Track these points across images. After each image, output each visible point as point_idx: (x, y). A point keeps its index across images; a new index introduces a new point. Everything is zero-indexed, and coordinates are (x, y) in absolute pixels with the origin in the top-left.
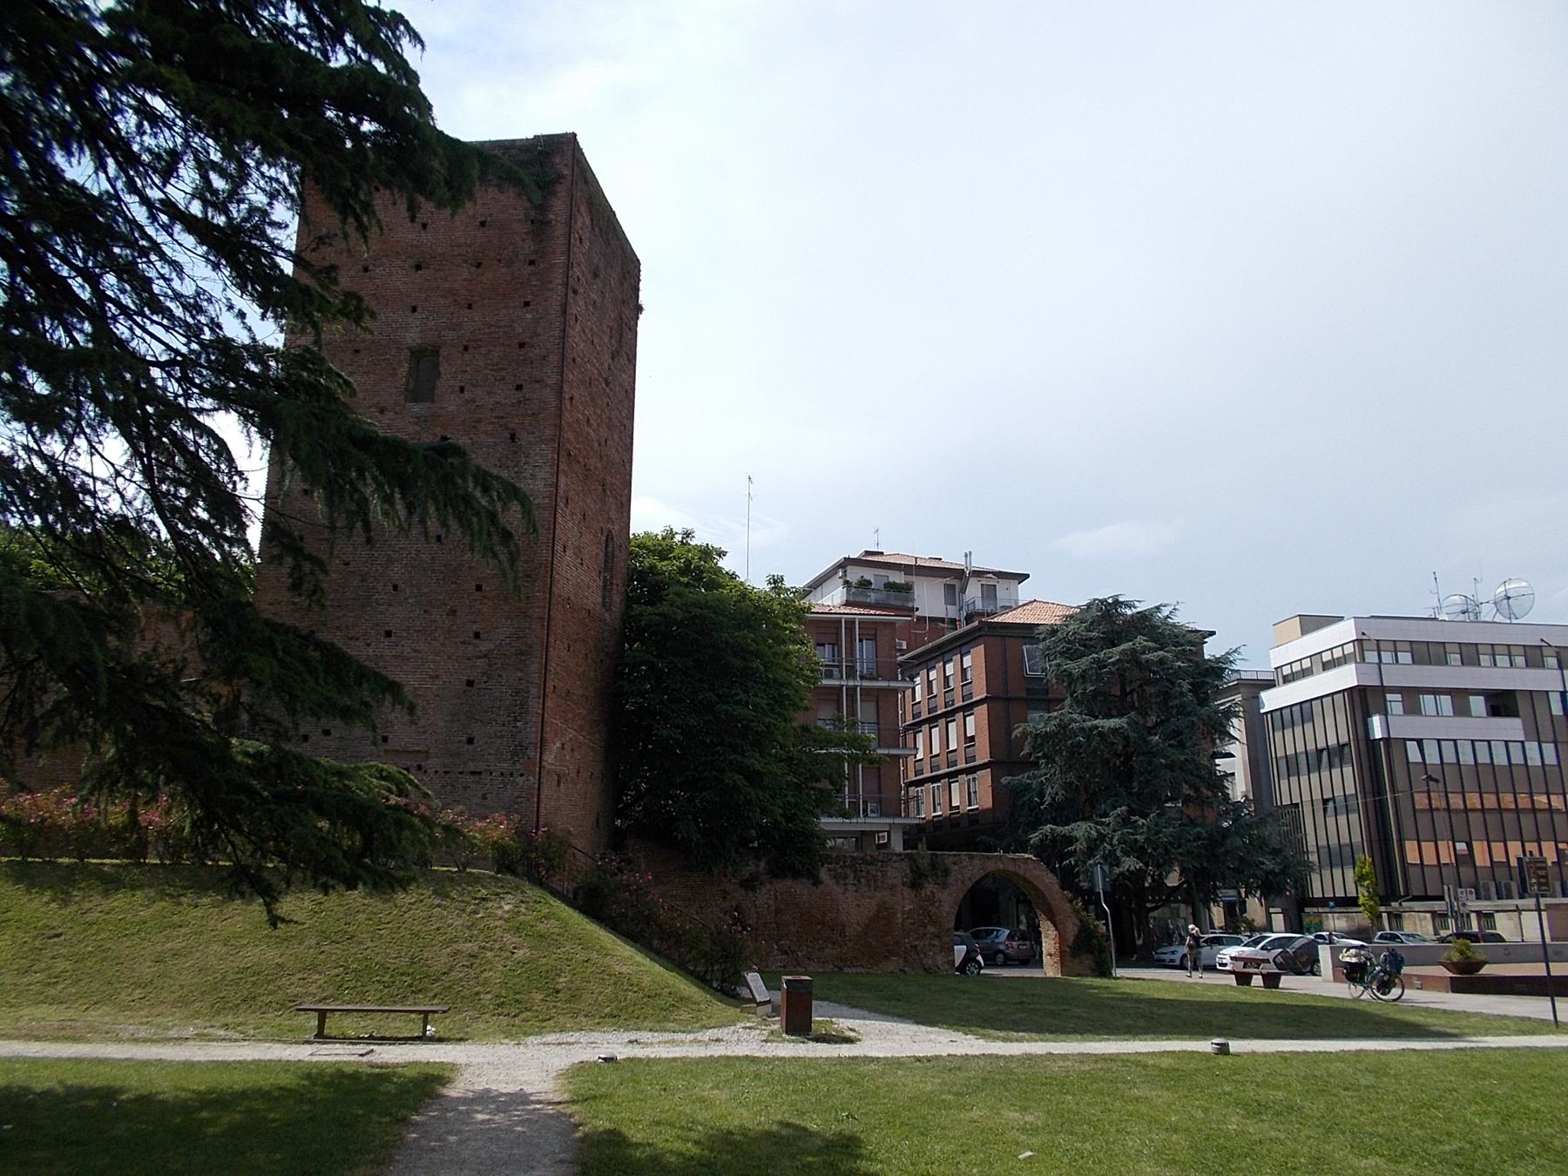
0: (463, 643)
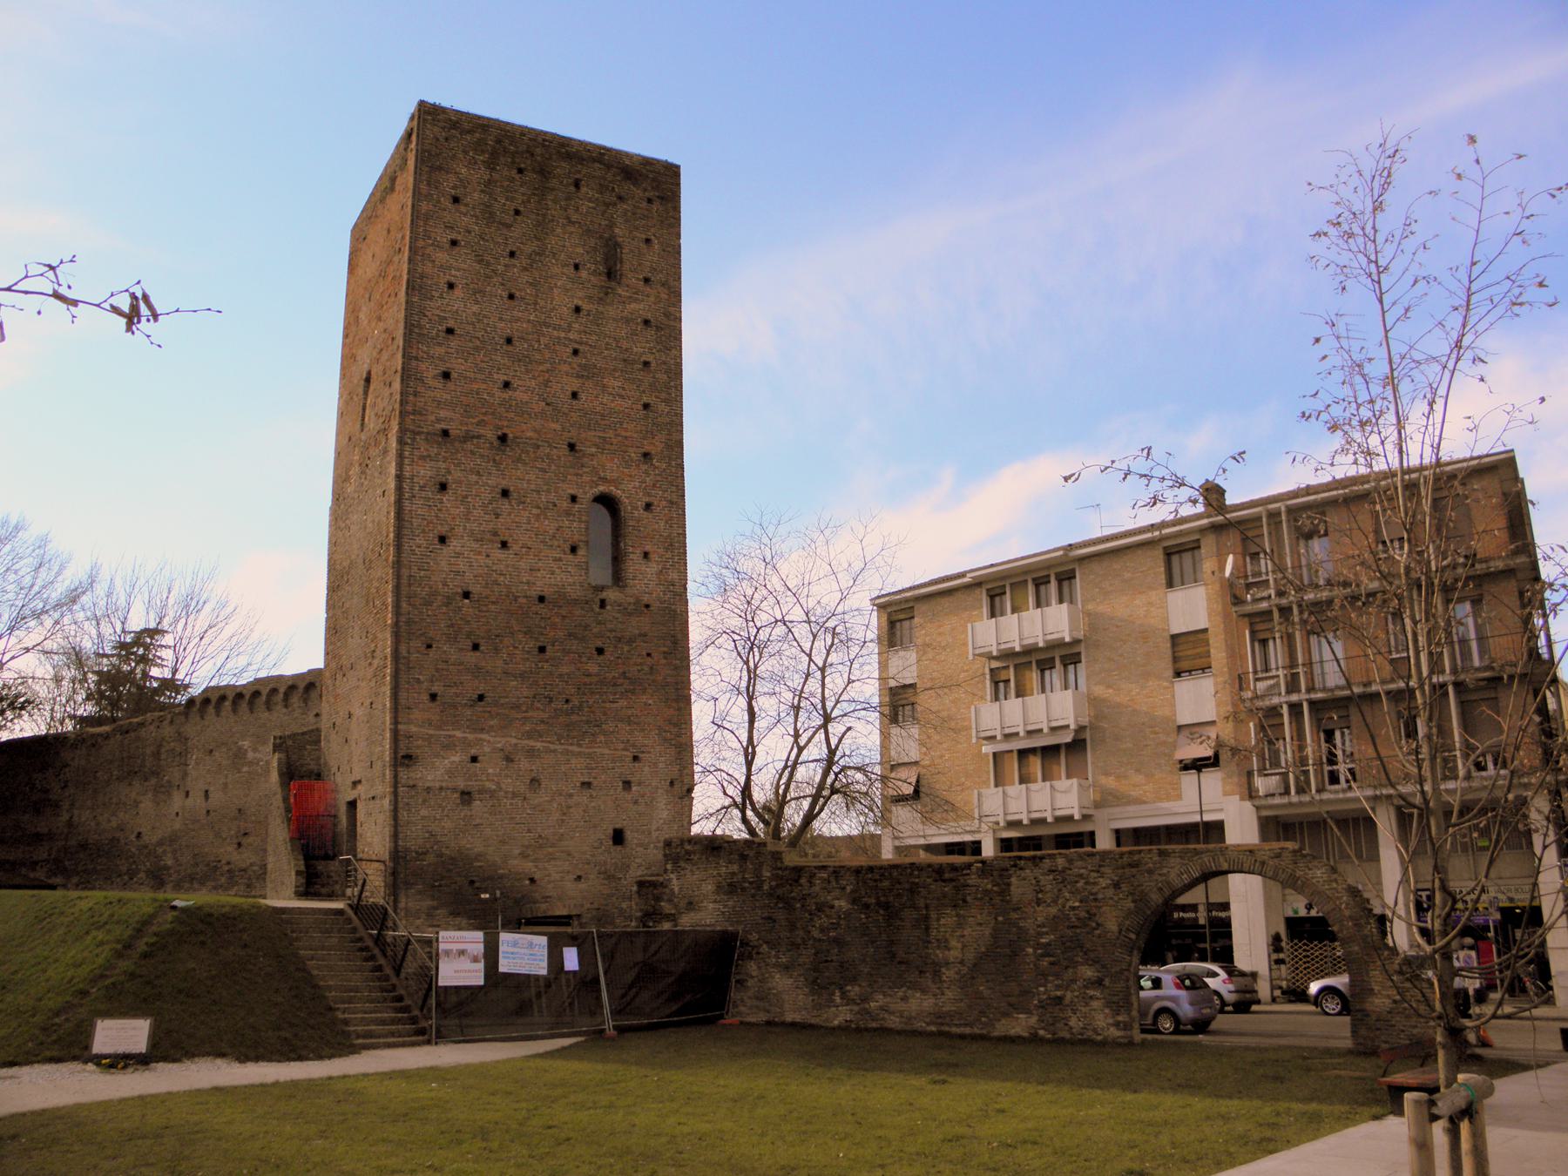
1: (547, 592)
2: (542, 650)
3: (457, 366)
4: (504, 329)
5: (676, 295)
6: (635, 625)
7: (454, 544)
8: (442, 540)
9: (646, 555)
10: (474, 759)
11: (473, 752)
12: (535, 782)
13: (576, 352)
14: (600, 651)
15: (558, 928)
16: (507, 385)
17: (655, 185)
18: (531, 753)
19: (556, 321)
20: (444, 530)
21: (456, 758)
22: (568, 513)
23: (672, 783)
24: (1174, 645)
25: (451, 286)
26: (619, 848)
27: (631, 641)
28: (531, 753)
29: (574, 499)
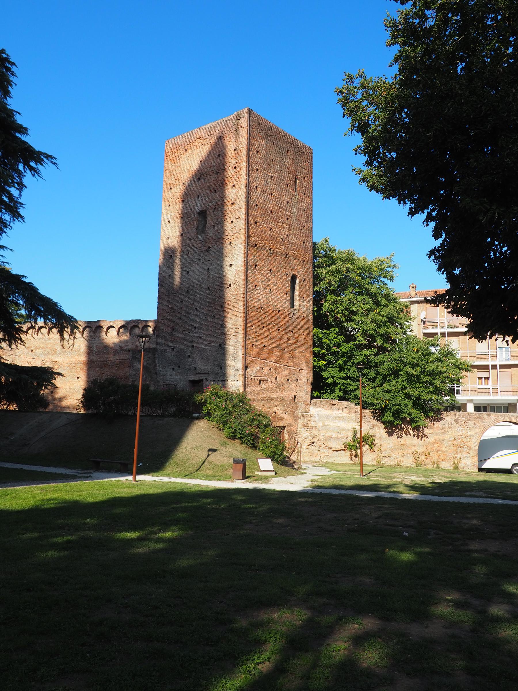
0: (218, 329)
11: (262, 366)
28: (276, 369)
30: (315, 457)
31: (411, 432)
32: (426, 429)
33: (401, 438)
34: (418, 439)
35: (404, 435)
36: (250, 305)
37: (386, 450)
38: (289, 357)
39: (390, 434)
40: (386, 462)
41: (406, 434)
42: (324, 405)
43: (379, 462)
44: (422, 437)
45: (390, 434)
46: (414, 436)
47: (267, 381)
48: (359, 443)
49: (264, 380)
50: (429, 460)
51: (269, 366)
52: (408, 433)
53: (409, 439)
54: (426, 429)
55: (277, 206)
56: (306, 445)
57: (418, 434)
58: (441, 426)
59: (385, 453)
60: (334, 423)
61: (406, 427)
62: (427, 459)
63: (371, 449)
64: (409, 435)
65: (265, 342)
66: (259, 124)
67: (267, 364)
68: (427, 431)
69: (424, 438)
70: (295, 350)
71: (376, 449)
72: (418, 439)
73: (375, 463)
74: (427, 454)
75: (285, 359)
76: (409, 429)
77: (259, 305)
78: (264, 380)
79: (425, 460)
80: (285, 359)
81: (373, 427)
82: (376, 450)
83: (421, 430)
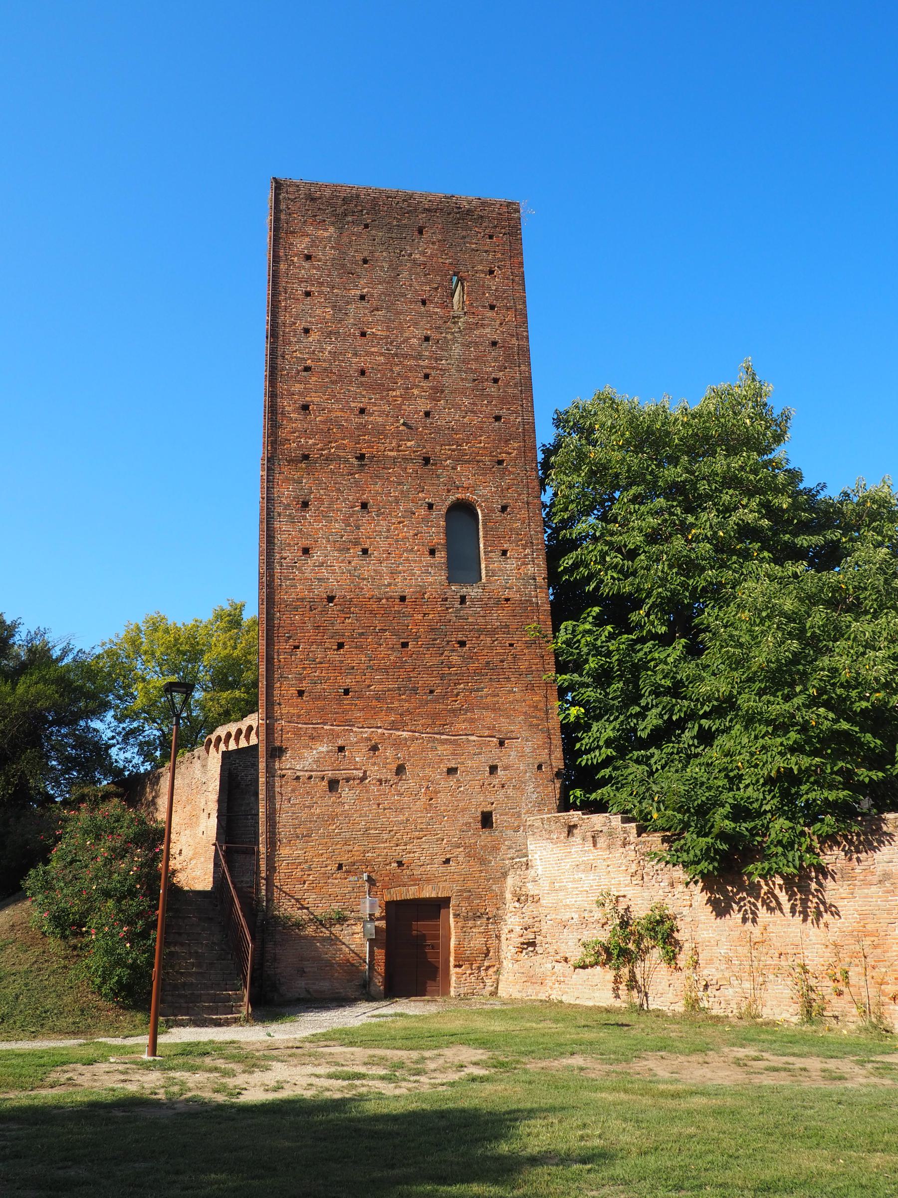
1: (407, 592)
2: (405, 645)
3: (314, 398)
4: (358, 362)
5: (523, 316)
6: (498, 617)
7: (317, 556)
8: (306, 551)
9: (504, 553)
10: (341, 749)
11: (340, 742)
12: (400, 770)
13: (427, 376)
14: (462, 644)
15: (267, 906)
16: (362, 411)
17: (501, 225)
18: (398, 744)
19: (405, 349)
20: (305, 543)
21: (324, 749)
22: (425, 520)
23: (540, 767)
24: (457, 216)
25: (307, 331)
26: (487, 831)
27: (494, 631)
28: (398, 744)
29: (430, 506)
30: (537, 987)
31: (783, 897)
32: (829, 883)
33: (754, 921)
34: (805, 920)
35: (762, 912)
36: (284, 595)
37: (710, 961)
38: (453, 711)
39: (721, 909)
40: (713, 1004)
41: (771, 909)
42: (550, 832)
43: (693, 1004)
44: (819, 915)
45: (721, 909)
46: (793, 911)
47: (363, 779)
48: (631, 943)
49: (348, 780)
50: (847, 997)
51: (369, 739)
52: (773, 904)
53: (781, 926)
54: (829, 883)
55: (381, 354)
56: (514, 951)
57: (804, 902)
58: (879, 869)
59: (707, 972)
60: (574, 881)
61: (767, 885)
62: (840, 994)
63: (671, 958)
64: (778, 912)
65: (348, 681)
66: (313, 200)
67: (356, 735)
68: (833, 891)
69: (827, 917)
70: (481, 689)
71: (683, 959)
72: (805, 920)
73: (680, 1008)
74: (839, 976)
75: (435, 716)
76: (777, 891)
77: (320, 591)
78: (348, 780)
79: (835, 999)
80: (435, 716)
81: (672, 885)
82: (681, 964)
83: (814, 886)
